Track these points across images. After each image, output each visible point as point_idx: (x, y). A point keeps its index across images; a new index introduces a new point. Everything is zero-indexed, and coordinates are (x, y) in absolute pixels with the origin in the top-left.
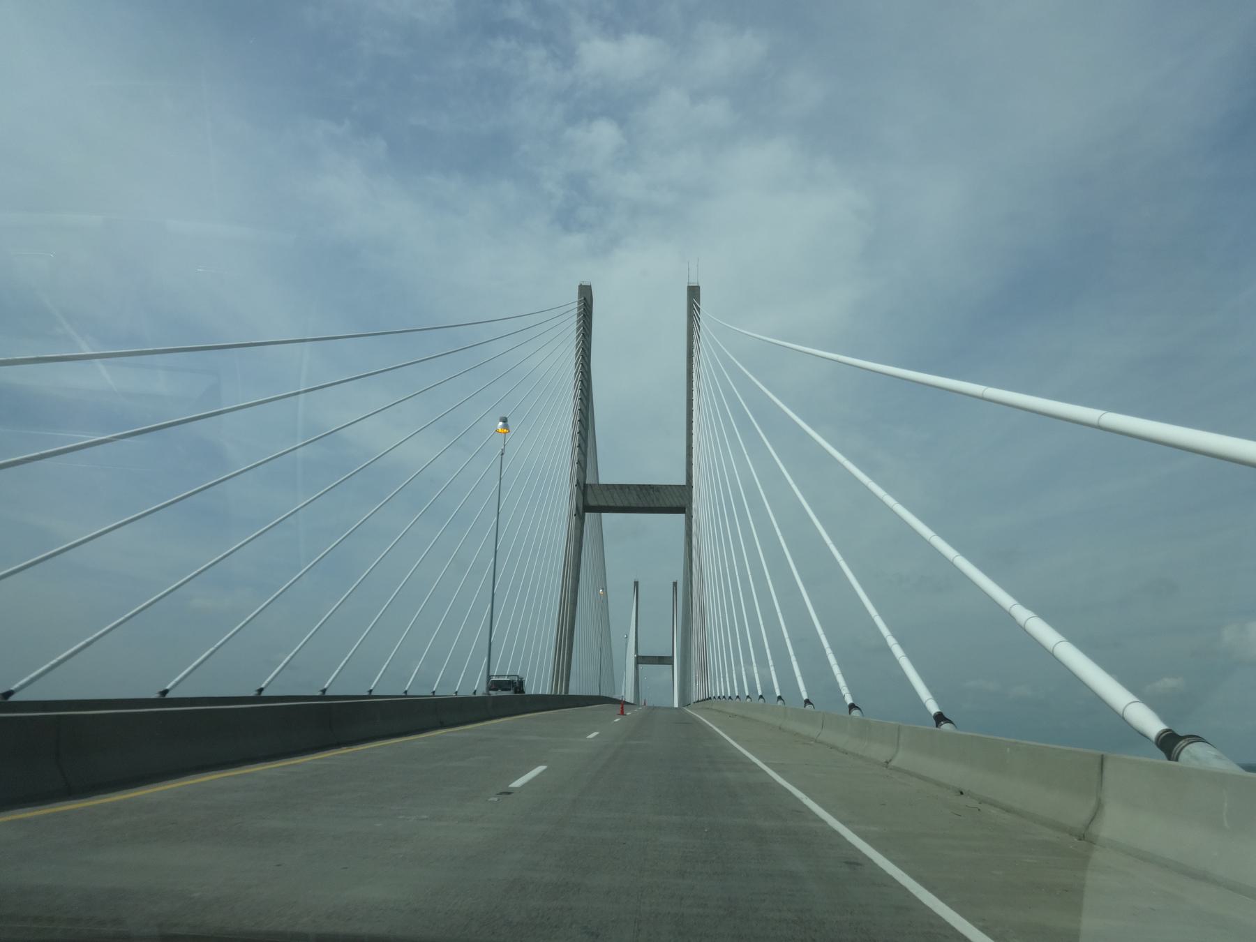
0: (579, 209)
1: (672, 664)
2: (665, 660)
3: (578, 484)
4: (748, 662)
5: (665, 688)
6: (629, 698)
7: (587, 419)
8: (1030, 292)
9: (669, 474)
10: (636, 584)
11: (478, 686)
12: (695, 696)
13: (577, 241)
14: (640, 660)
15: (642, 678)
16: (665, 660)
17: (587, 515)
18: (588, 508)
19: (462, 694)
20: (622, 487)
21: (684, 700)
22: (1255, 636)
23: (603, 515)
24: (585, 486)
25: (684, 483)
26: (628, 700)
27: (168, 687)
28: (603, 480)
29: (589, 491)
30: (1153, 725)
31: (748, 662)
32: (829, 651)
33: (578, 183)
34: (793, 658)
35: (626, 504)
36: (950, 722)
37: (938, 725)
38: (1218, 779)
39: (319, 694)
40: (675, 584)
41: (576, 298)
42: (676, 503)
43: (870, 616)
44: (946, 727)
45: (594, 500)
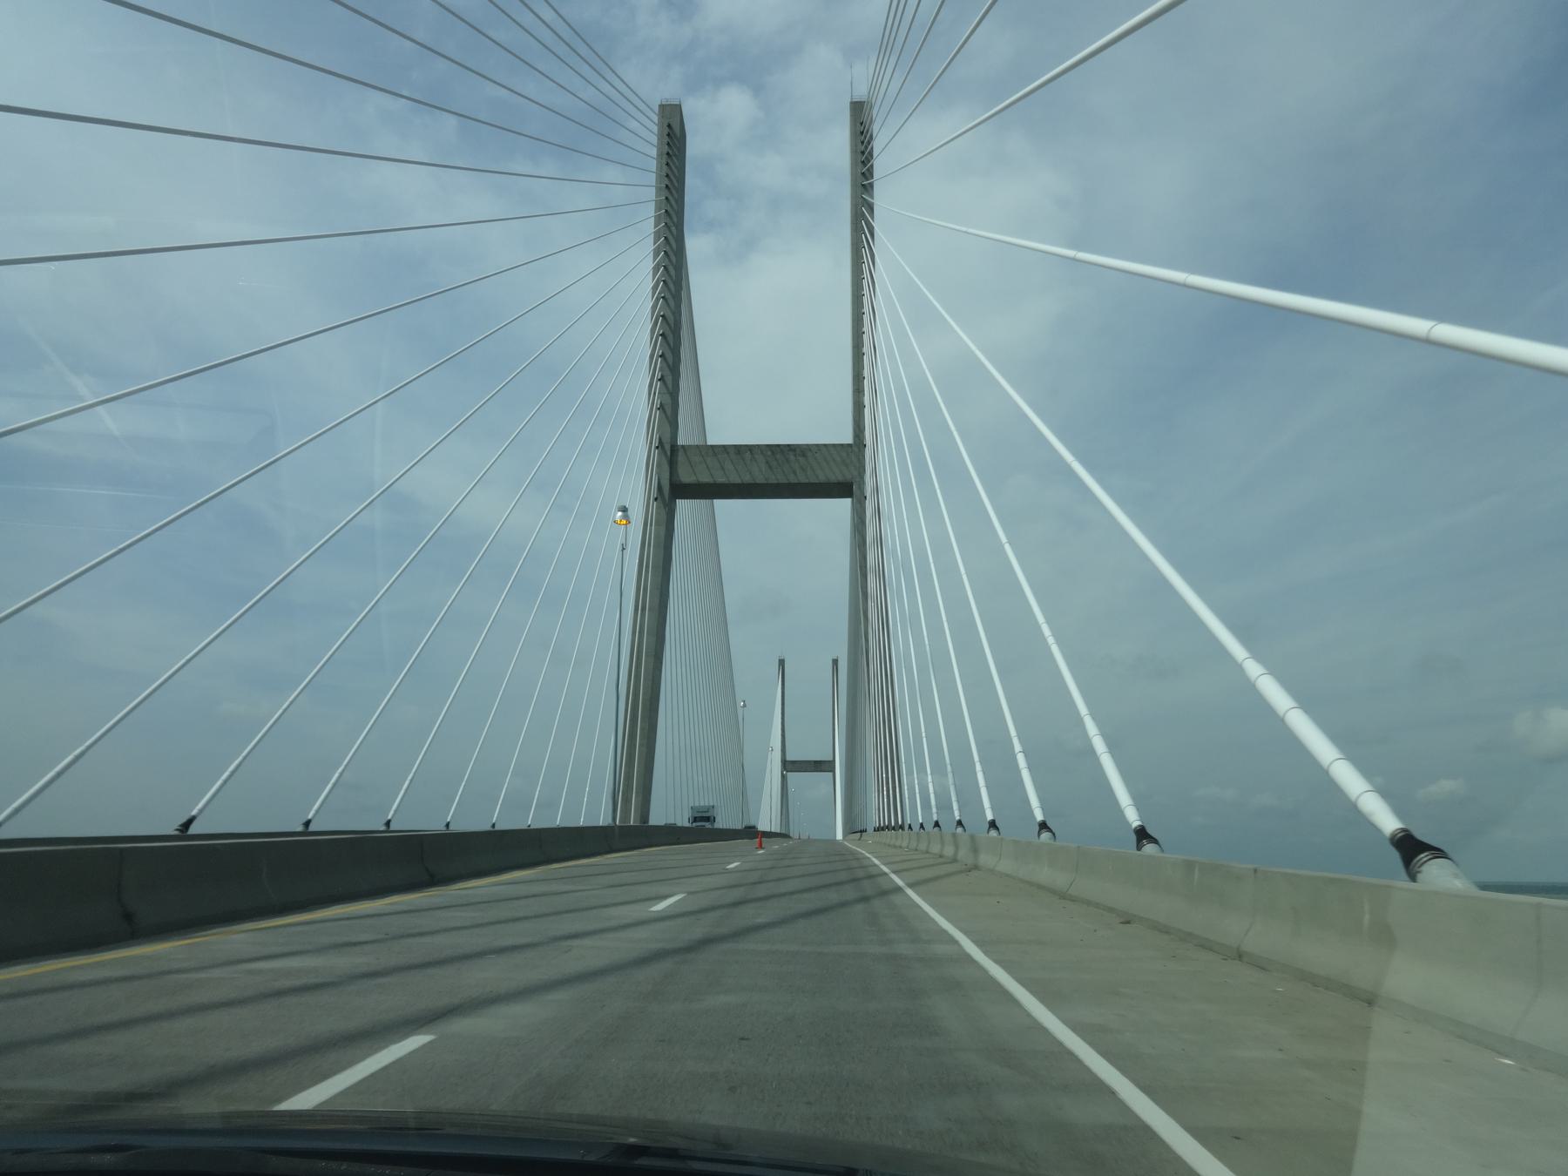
1: (833, 770)
2: (824, 766)
3: (660, 446)
5: (825, 811)
6: (767, 820)
7: (677, 313)
9: (826, 425)
10: (782, 663)
11: (739, 827)
12: (873, 820)
14: (788, 766)
15: (791, 789)
16: (824, 766)
19: (408, 822)
20: (739, 450)
21: (854, 828)
22: (1567, 723)
24: (674, 448)
26: (763, 826)
29: (681, 457)
34: (978, 767)
35: (747, 479)
36: (1155, 841)
37: (1139, 848)
39: (300, 829)
40: (835, 662)
42: (835, 475)
43: (1078, 713)
44: (1149, 848)
45: (690, 475)
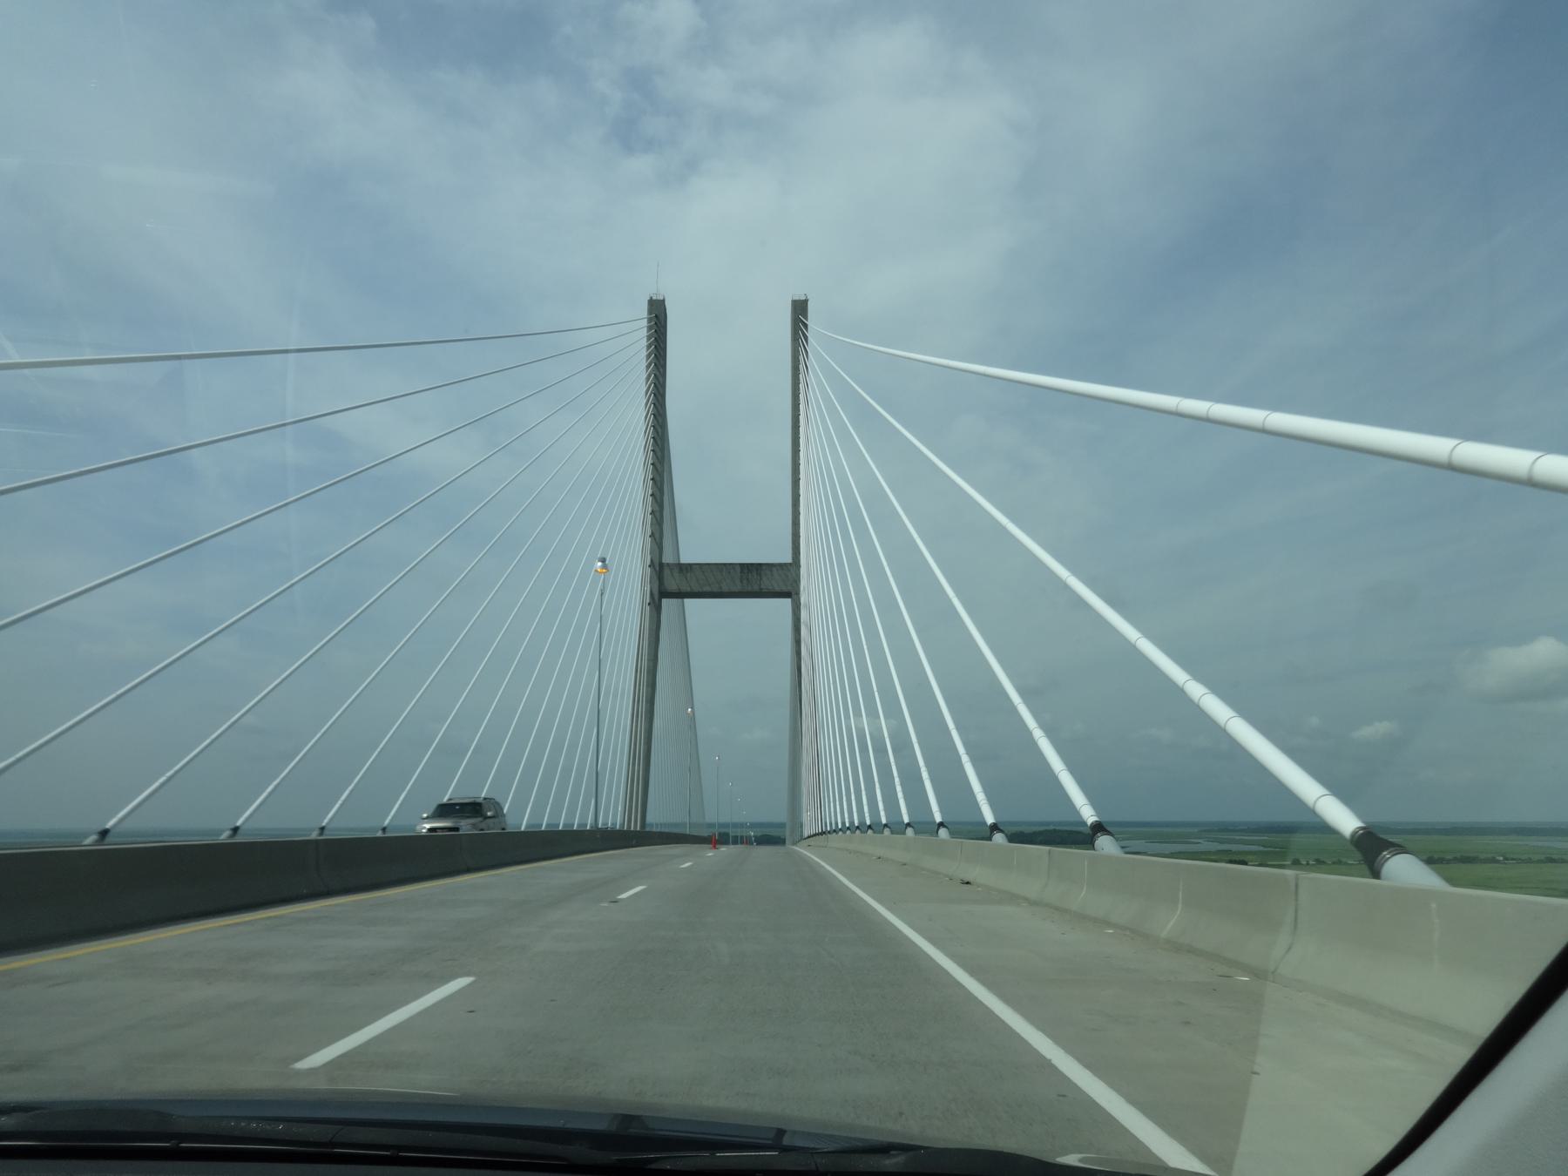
0: (645, 122)
3: (652, 565)
4: (858, 714)
8: (1218, 244)
13: (641, 165)
17: (664, 601)
18: (665, 594)
23: (686, 601)
24: (661, 565)
25: (789, 560)
27: (109, 825)
28: (686, 558)
29: (667, 572)
30: (1346, 821)
31: (858, 714)
32: (965, 759)
33: (640, 81)
38: (1420, 897)
41: (645, 314)
45: (673, 582)
